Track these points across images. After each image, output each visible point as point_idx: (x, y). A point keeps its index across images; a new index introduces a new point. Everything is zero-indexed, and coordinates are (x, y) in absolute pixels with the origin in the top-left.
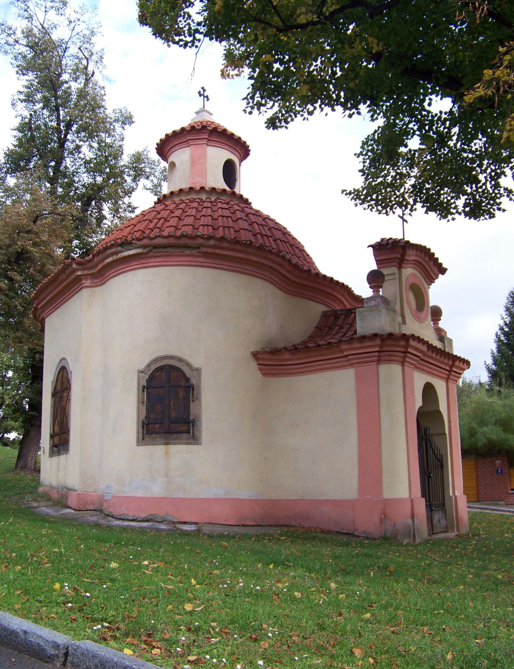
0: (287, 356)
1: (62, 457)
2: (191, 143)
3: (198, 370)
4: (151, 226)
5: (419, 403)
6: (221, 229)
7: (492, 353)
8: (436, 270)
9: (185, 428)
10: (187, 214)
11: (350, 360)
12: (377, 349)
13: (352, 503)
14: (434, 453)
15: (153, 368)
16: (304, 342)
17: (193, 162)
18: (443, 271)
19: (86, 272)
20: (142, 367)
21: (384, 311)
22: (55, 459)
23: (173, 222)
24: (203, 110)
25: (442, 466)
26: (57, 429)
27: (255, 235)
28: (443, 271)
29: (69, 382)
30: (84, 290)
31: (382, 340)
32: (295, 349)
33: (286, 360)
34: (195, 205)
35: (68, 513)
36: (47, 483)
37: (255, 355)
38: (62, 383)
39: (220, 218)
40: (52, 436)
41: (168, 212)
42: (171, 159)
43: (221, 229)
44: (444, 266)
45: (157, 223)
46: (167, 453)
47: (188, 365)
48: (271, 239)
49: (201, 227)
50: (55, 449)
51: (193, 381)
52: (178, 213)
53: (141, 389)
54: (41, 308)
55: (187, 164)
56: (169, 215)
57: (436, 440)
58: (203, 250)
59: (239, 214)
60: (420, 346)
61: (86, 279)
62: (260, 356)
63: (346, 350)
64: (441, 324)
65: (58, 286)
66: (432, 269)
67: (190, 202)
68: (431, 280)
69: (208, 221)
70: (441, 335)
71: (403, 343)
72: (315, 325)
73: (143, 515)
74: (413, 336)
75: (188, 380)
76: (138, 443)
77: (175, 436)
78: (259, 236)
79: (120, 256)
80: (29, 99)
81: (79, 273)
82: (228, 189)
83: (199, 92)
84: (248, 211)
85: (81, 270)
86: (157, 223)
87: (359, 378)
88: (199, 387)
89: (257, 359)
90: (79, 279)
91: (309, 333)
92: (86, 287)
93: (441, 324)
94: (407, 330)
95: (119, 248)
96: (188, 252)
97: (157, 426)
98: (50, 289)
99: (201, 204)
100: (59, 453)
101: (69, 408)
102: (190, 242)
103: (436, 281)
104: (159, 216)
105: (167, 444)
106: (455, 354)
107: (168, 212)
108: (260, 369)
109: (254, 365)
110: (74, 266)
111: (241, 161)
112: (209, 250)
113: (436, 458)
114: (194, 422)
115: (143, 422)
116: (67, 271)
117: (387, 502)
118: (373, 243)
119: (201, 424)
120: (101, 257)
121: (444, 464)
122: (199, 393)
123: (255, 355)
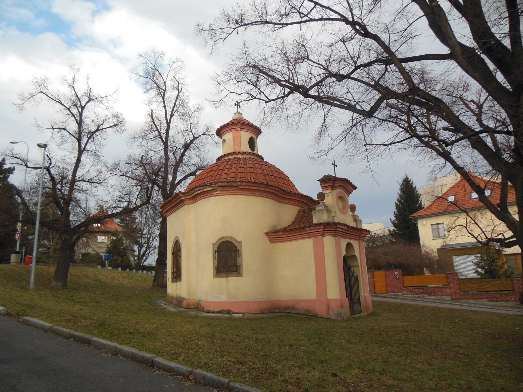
0: (281, 233)
1: (178, 283)
2: (233, 130)
3: (240, 242)
4: (216, 173)
5: (344, 253)
6: (249, 174)
7: (394, 212)
8: (351, 188)
9: (235, 269)
10: (233, 167)
11: (310, 235)
12: (322, 230)
13: (314, 301)
14: (353, 275)
15: (220, 242)
16: (289, 226)
17: (234, 139)
18: (355, 188)
19: (186, 198)
20: (214, 242)
21: (325, 212)
22: (175, 284)
23: (226, 171)
24: (238, 112)
25: (358, 282)
26: (175, 270)
27: (265, 175)
28: (355, 188)
29: (180, 248)
30: (186, 206)
31: (324, 226)
32: (285, 230)
33: (281, 235)
34: (236, 162)
35: (182, 310)
36: (171, 295)
37: (267, 234)
38: (177, 248)
39: (248, 168)
40: (173, 273)
41: (223, 166)
42: (224, 137)
43: (249, 174)
44: (356, 186)
45: (218, 172)
46: (227, 281)
47: (236, 241)
48: (272, 177)
49: (239, 173)
50: (175, 279)
51: (238, 248)
52: (228, 166)
53: (214, 252)
54: (165, 212)
55: (231, 141)
56: (224, 168)
57: (355, 269)
58: (241, 187)
59: (257, 166)
60: (343, 227)
61: (186, 201)
62: (269, 234)
63: (308, 230)
64: (356, 213)
65: (172, 204)
66: (349, 188)
67: (234, 160)
68: (349, 193)
69: (242, 170)
70: (356, 219)
71: (334, 227)
72: (295, 217)
73: (217, 310)
74: (339, 223)
75: (236, 247)
76: (214, 277)
77: (231, 273)
78: (267, 175)
79: (202, 191)
80: (150, 103)
81: (183, 198)
82: (250, 151)
83: (235, 104)
84: (261, 163)
85: (184, 196)
86: (218, 172)
87: (315, 244)
88: (241, 251)
89: (268, 236)
90: (183, 201)
91: (292, 221)
92: (187, 204)
93: (356, 213)
94: (336, 220)
95: (202, 188)
96: (233, 188)
97: (222, 269)
98: (169, 204)
99: (239, 161)
100: (176, 281)
101: (181, 260)
102: (234, 184)
103: (352, 193)
104: (219, 168)
105: (227, 277)
106: (363, 228)
107: (223, 166)
108: (269, 240)
109: (266, 239)
110: (180, 195)
111: (257, 136)
112: (243, 187)
113: (355, 277)
114: (239, 266)
115: (216, 267)
116: (178, 197)
117: (328, 301)
118: (319, 178)
119: (242, 267)
120: (193, 191)
121: (359, 280)
122: (241, 253)
123: (267, 234)
